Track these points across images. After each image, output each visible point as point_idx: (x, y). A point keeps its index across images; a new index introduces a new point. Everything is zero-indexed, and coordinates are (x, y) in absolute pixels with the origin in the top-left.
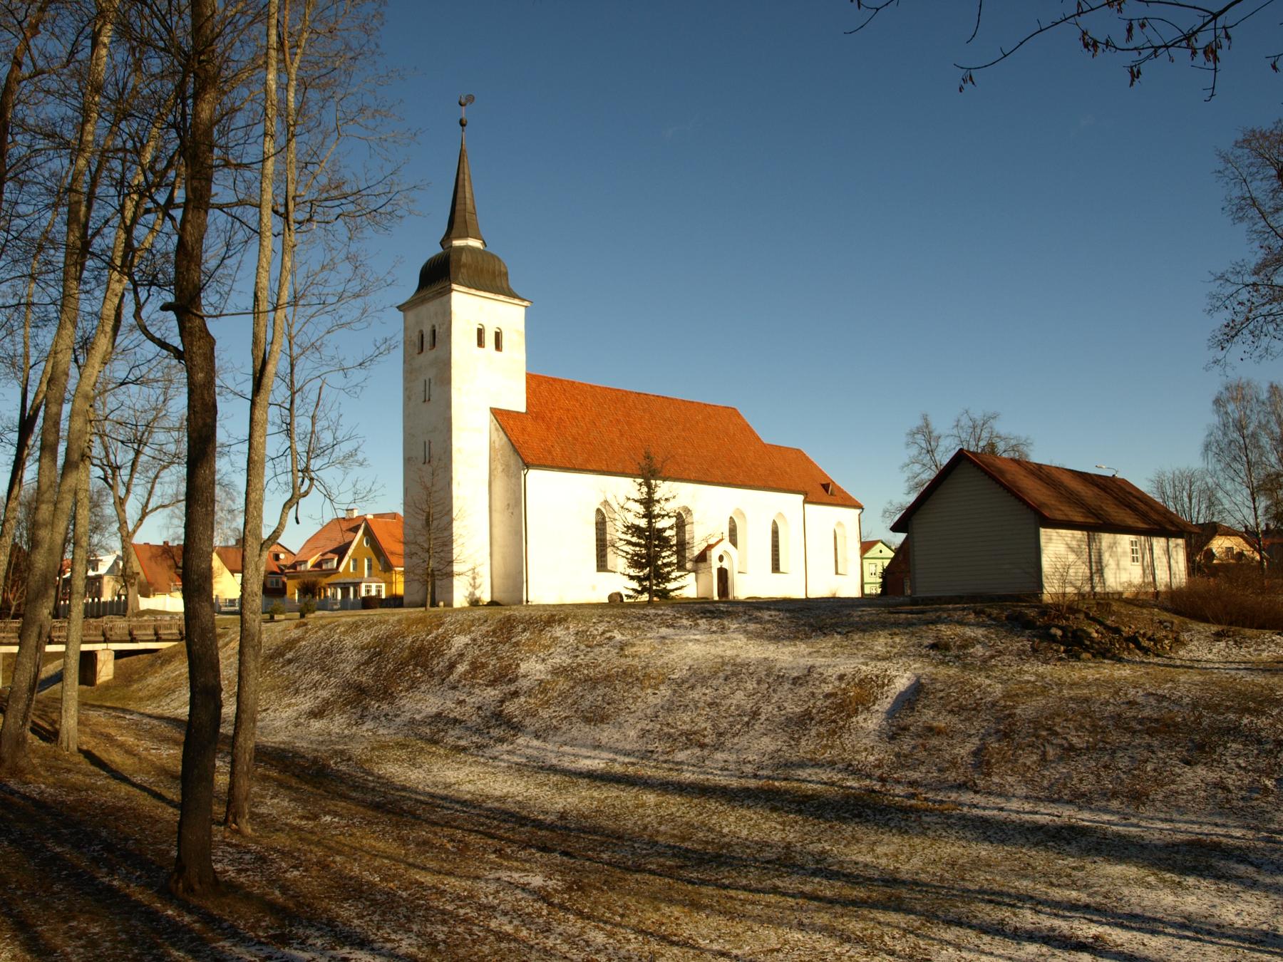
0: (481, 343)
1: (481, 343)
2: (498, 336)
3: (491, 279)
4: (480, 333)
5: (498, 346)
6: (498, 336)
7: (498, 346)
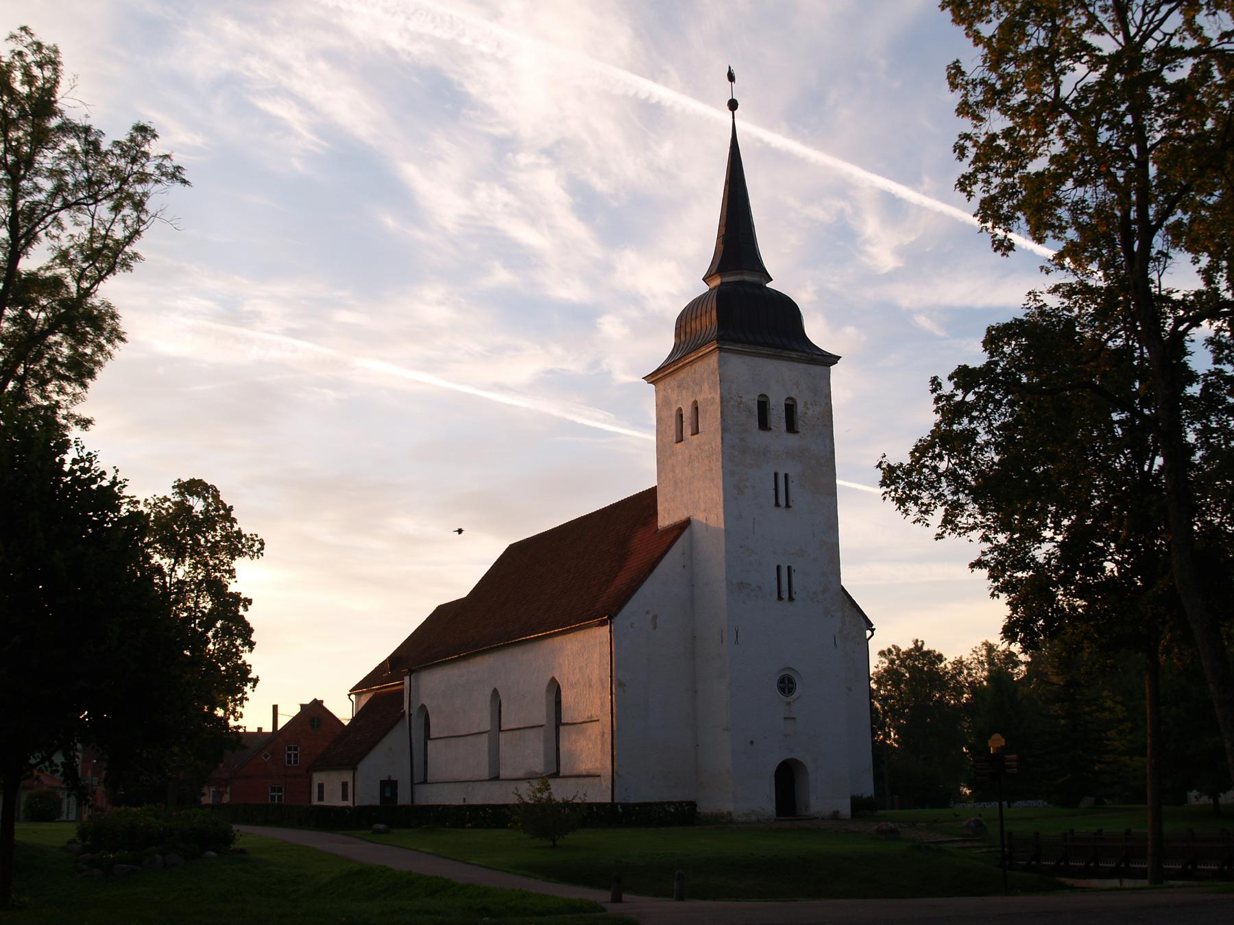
0: (764, 424)
1: (764, 424)
2: (790, 408)
4: (763, 405)
5: (791, 427)
6: (790, 408)
7: (791, 427)
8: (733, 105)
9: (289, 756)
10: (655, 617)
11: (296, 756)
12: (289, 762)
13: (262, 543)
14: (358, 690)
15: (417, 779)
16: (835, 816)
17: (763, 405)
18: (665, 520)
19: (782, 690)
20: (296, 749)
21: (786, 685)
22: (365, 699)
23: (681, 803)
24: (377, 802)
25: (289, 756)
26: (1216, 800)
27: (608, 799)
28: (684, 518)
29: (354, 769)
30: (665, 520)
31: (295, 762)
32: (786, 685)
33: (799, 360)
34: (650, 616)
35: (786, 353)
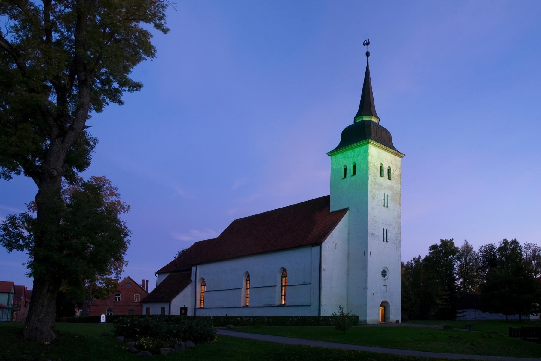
0: (381, 175)
2: (389, 171)
3: (385, 140)
4: (381, 168)
5: (389, 178)
6: (389, 171)
8: (368, 54)
9: (116, 298)
10: (336, 245)
11: (119, 298)
12: (116, 300)
13: (129, 206)
14: (159, 273)
15: (198, 306)
16: (397, 322)
17: (381, 168)
18: (334, 208)
19: (383, 275)
20: (119, 295)
21: (384, 273)
22: (163, 277)
23: (250, 317)
24: (179, 314)
25: (116, 298)
26: (520, 317)
27: (316, 314)
28: (345, 207)
29: (170, 302)
30: (334, 208)
31: (119, 300)
32: (384, 273)
33: (390, 152)
34: (334, 244)
35: (390, 149)
